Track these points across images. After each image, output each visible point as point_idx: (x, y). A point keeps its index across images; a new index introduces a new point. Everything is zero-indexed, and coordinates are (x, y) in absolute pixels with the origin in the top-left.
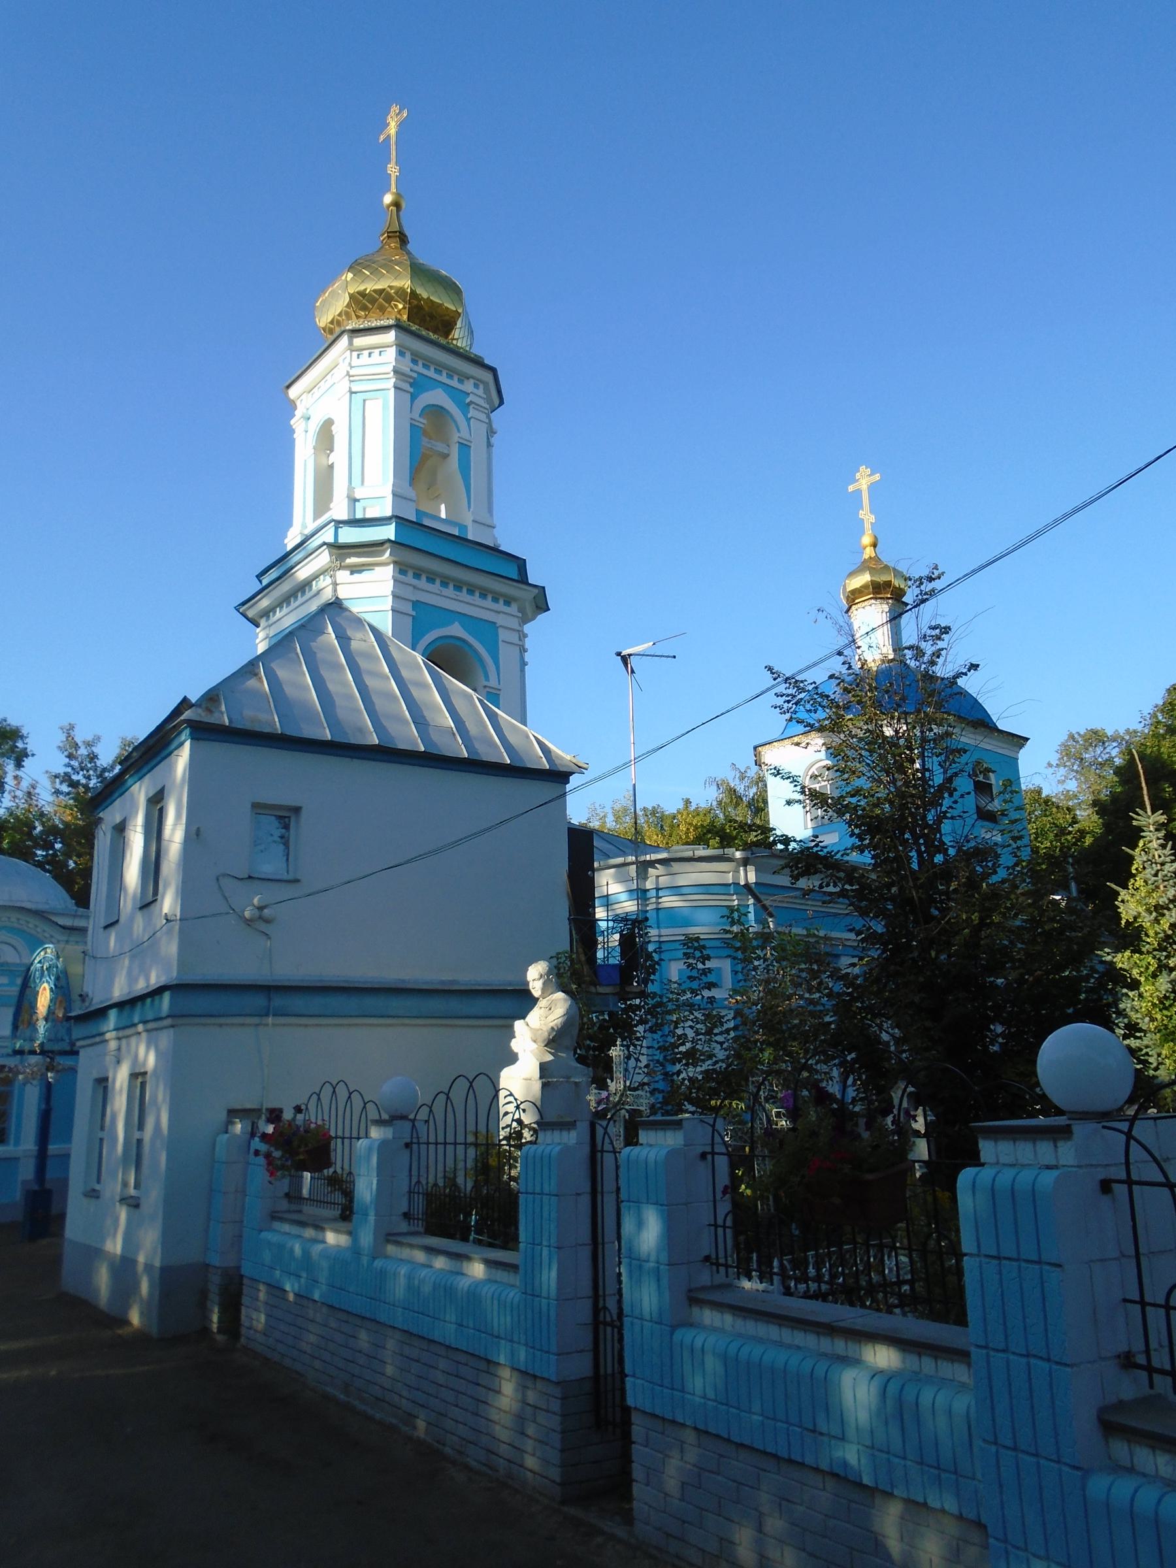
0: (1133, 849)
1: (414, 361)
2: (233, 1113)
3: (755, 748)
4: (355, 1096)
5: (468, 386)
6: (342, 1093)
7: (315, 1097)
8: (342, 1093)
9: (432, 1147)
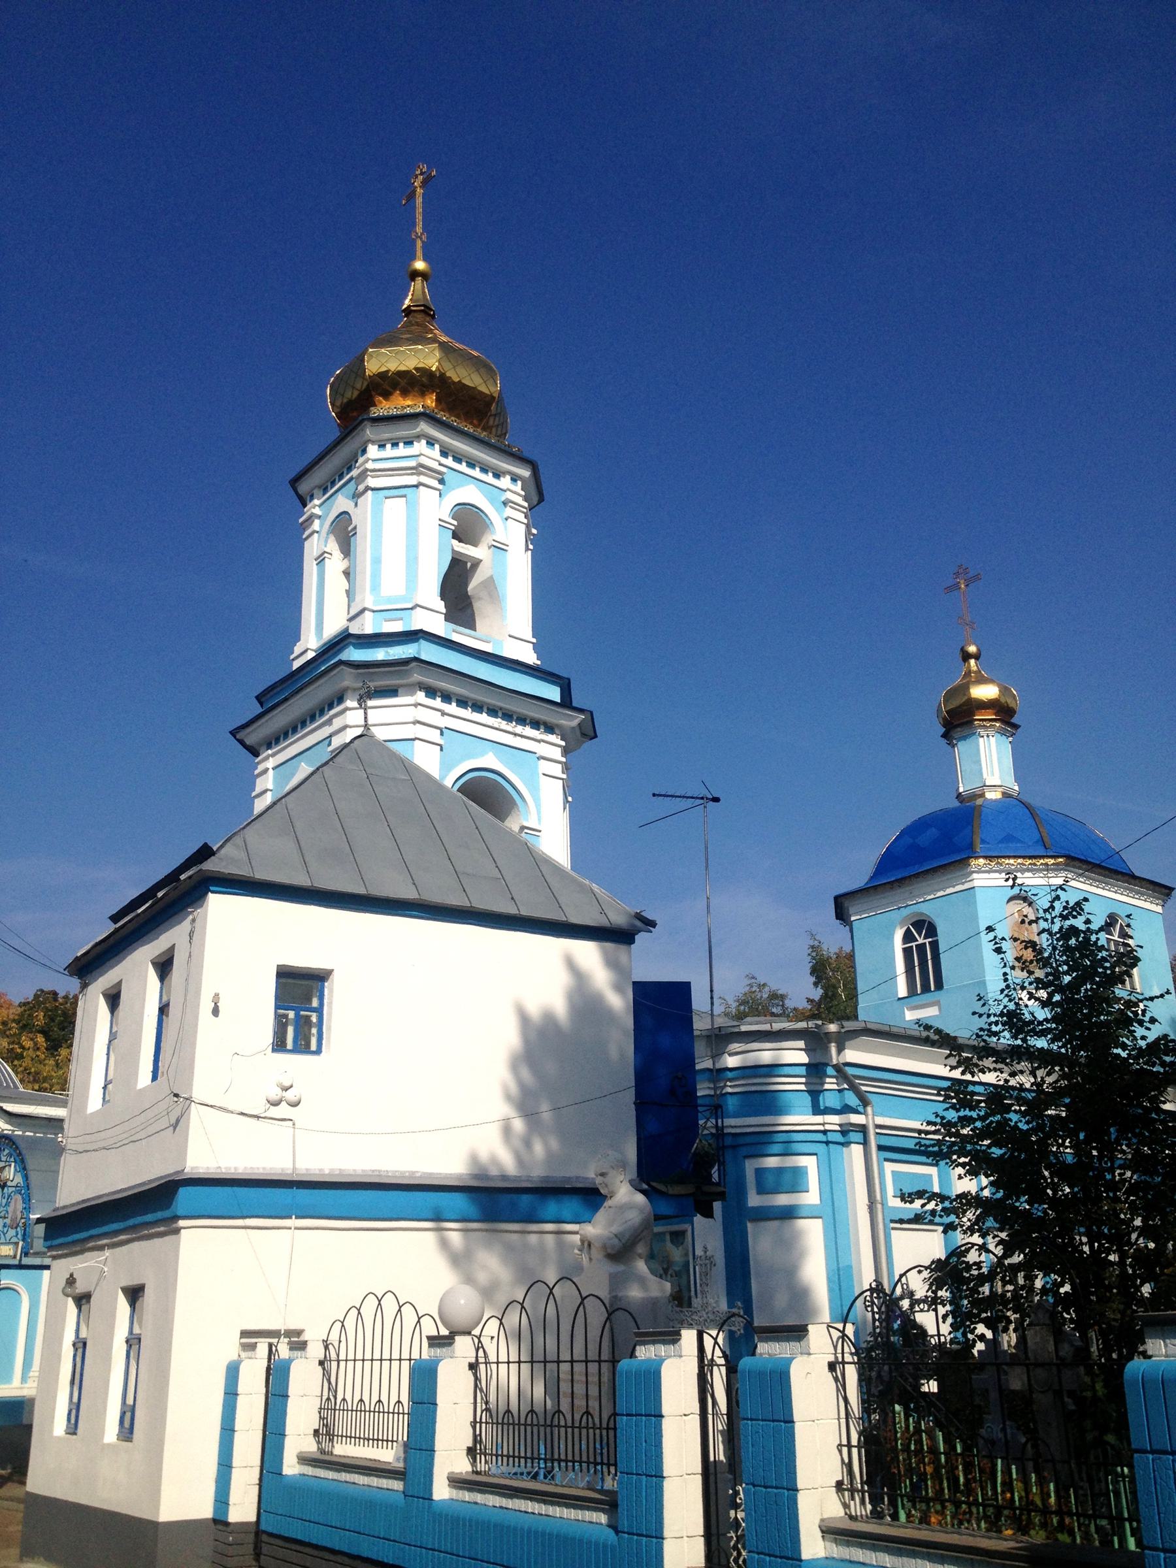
0: (475, 544)
1: (444, 453)
2: (250, 1336)
3: (836, 898)
4: (407, 1310)
5: (505, 482)
6: (390, 1305)
7: (354, 1312)
8: (390, 1305)
9: (359, 1364)
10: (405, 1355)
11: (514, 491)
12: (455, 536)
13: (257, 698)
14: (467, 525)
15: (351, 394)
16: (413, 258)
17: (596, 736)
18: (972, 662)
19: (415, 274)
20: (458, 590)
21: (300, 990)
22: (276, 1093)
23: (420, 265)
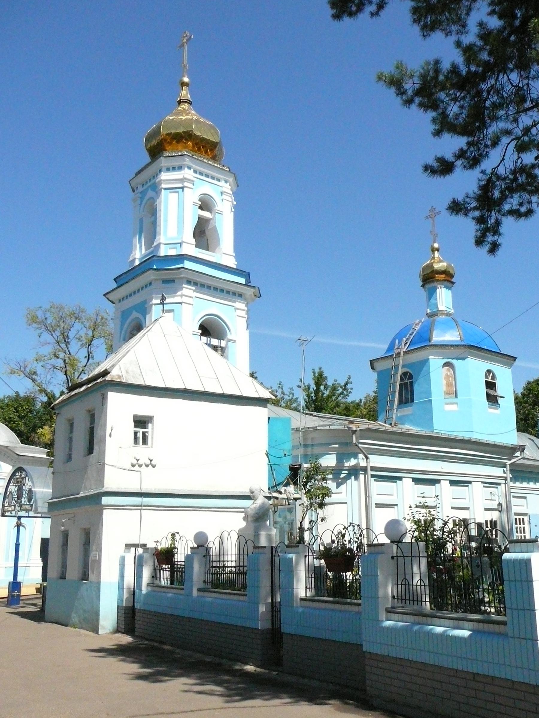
2: (128, 546)
10: (183, 552)
11: (227, 187)
12: (201, 208)
13: (115, 279)
14: (205, 204)
15: (154, 142)
16: (183, 76)
17: (261, 296)
18: (436, 253)
19: (183, 84)
20: (203, 233)
21: (141, 422)
22: (135, 462)
23: (186, 80)
